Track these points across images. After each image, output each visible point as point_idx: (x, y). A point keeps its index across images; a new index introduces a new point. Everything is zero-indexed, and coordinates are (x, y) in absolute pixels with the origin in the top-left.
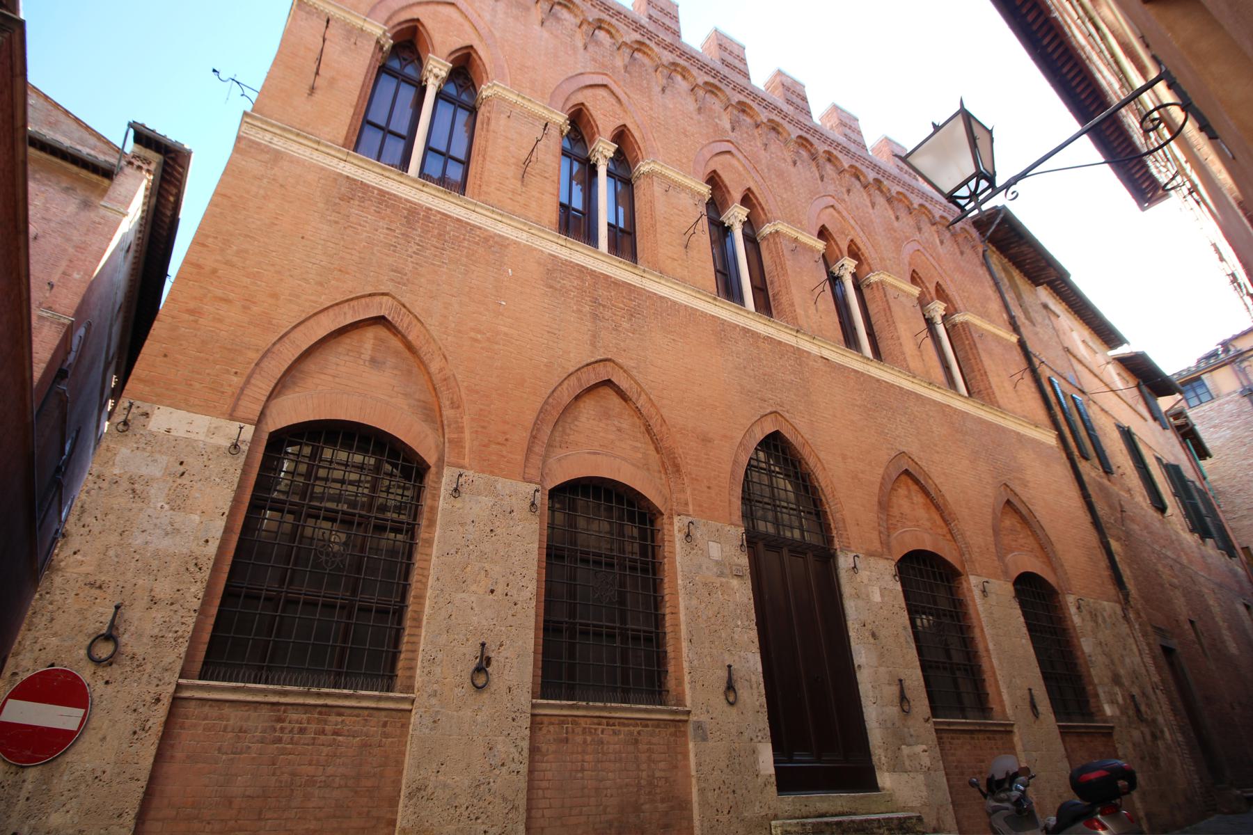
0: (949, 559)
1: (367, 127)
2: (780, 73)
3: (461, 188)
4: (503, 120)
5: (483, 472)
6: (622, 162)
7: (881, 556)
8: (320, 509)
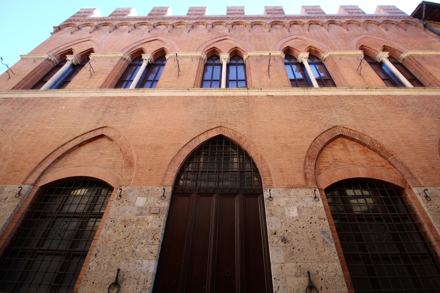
0: (387, 180)
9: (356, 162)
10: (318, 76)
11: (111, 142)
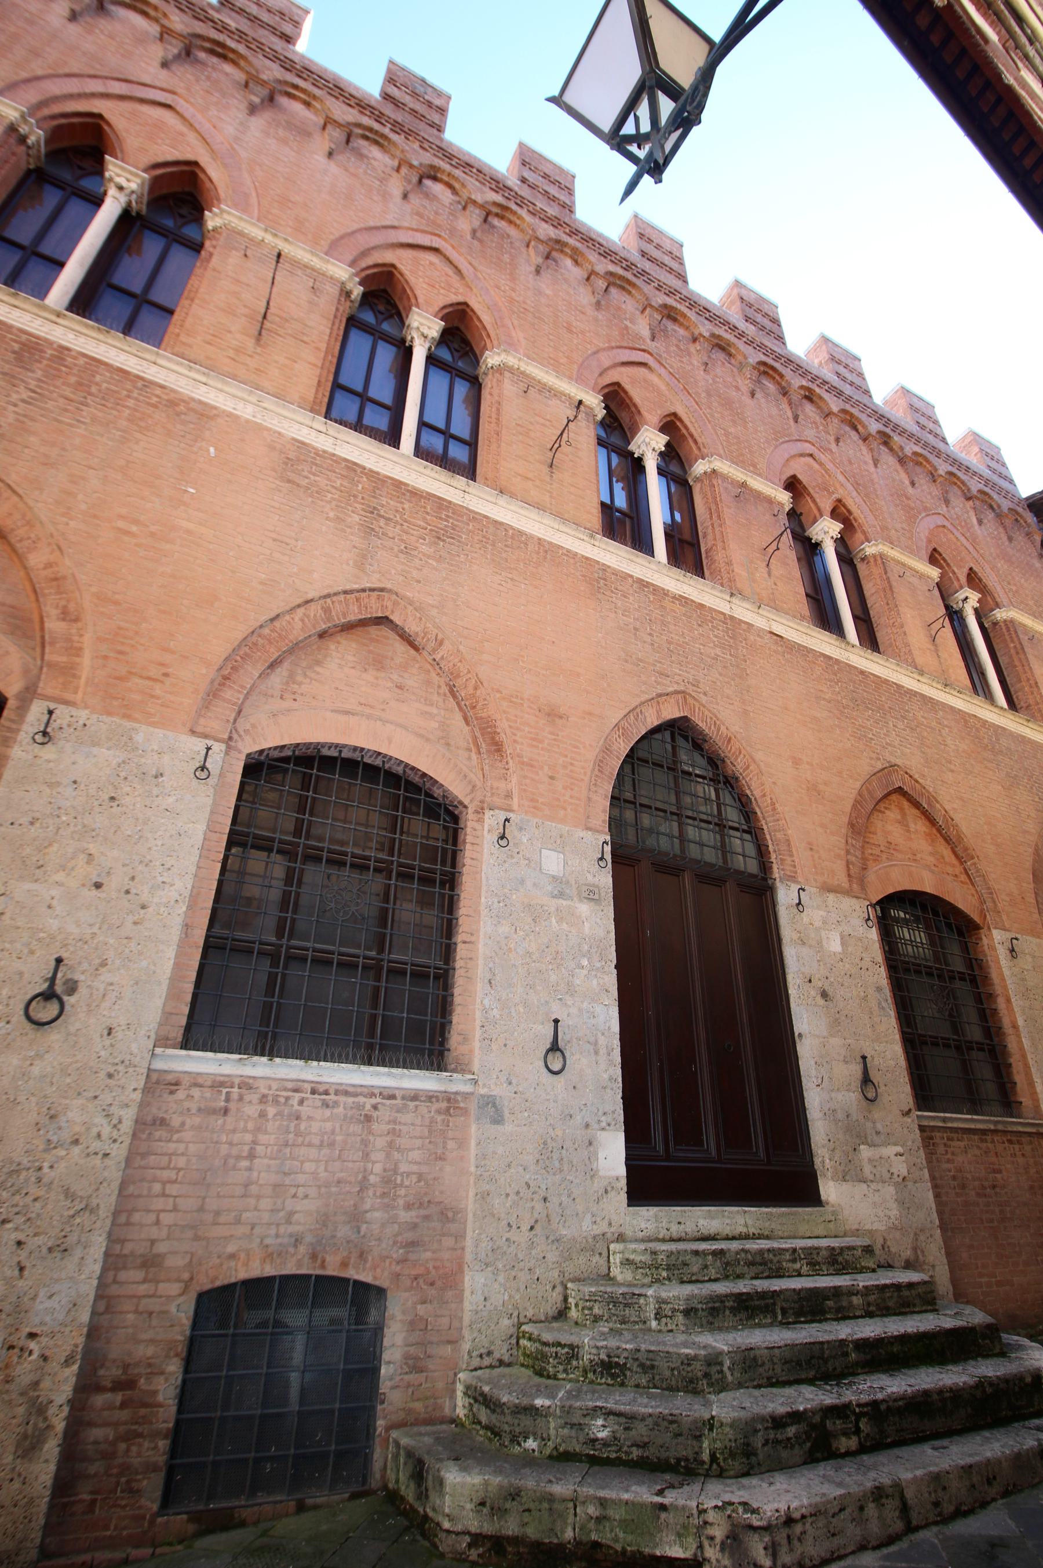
0: (960, 906)
1: (339, 395)
2: (737, 284)
3: (470, 471)
5: (109, 714)
6: (466, 354)
7: (848, 893)
8: (247, 835)
9: (919, 856)
11: (412, 652)
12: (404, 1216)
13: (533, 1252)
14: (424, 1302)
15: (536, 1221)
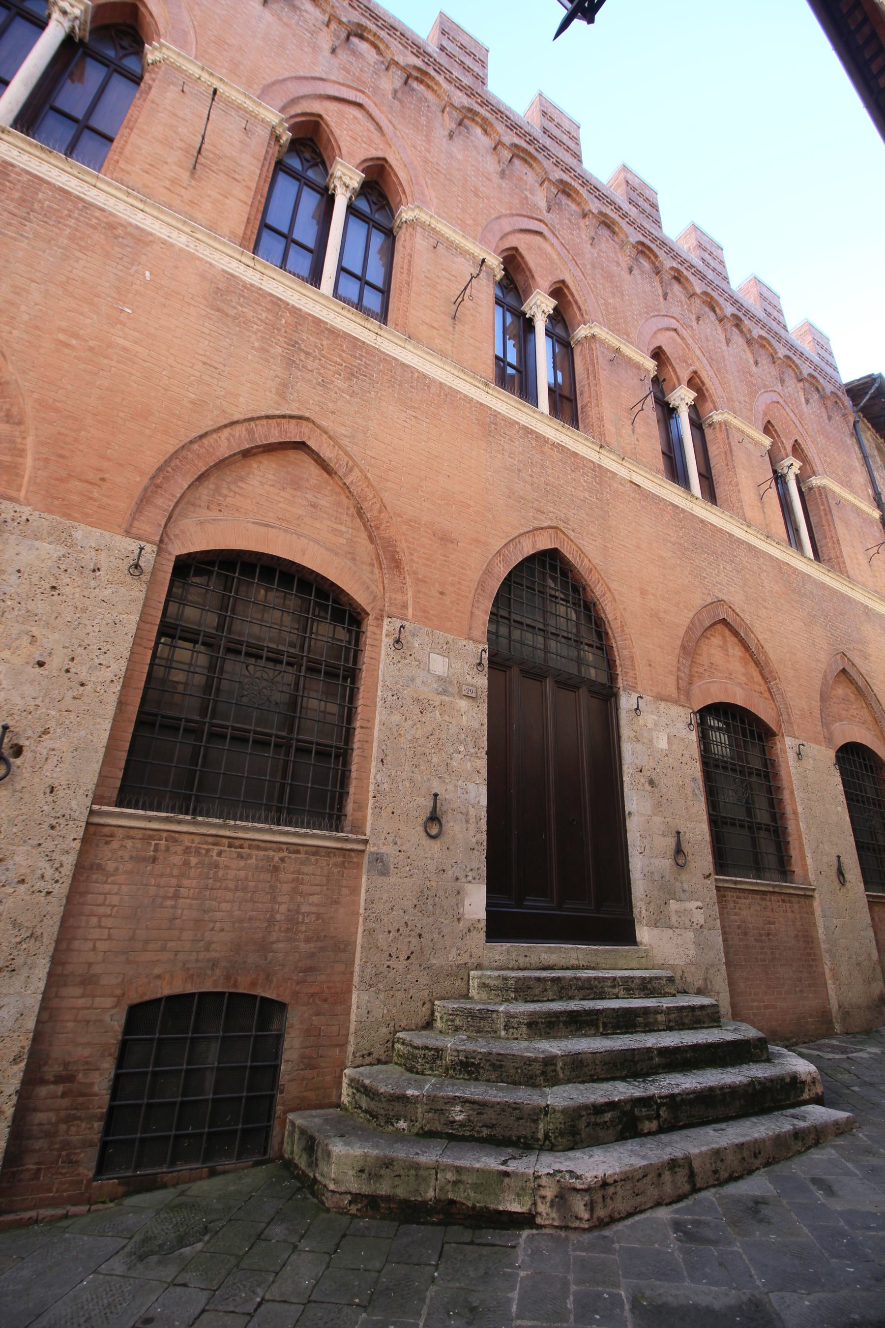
4: (173, 92)
5: (50, 512)
7: (676, 702)
10: (553, 382)
11: (325, 475)
12: (303, 947)
13: (409, 976)
14: (318, 1014)
15: (412, 953)
